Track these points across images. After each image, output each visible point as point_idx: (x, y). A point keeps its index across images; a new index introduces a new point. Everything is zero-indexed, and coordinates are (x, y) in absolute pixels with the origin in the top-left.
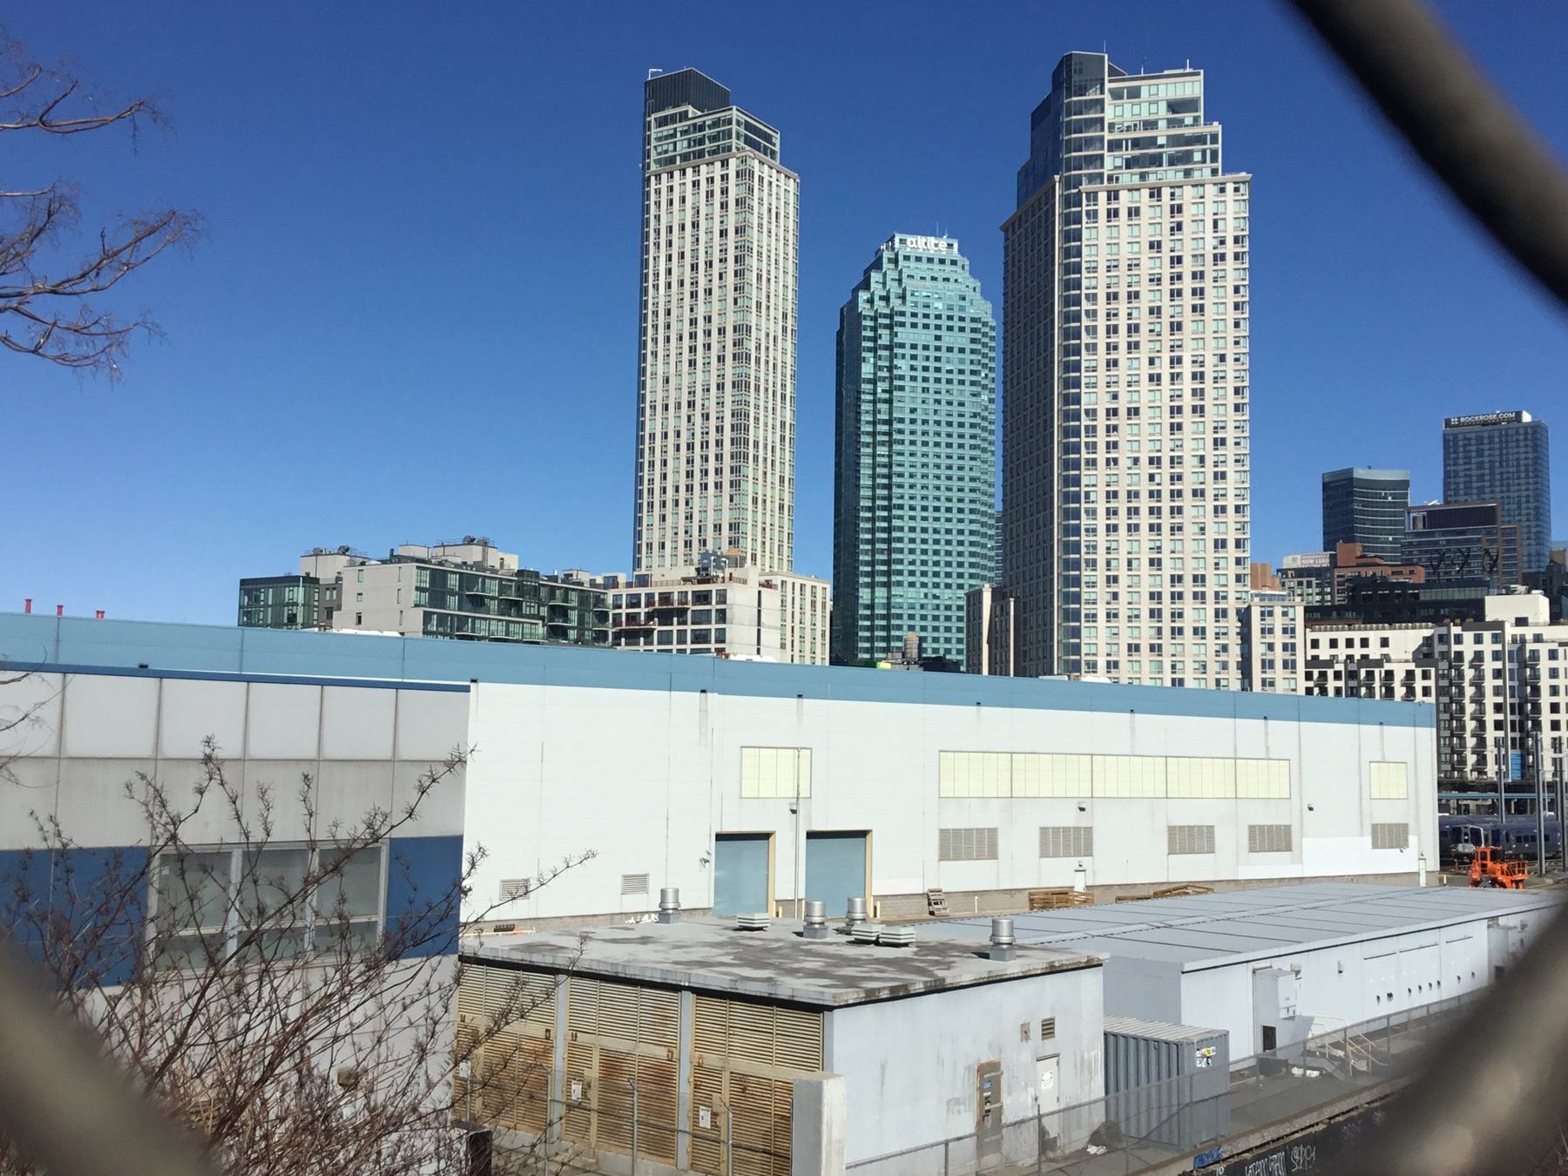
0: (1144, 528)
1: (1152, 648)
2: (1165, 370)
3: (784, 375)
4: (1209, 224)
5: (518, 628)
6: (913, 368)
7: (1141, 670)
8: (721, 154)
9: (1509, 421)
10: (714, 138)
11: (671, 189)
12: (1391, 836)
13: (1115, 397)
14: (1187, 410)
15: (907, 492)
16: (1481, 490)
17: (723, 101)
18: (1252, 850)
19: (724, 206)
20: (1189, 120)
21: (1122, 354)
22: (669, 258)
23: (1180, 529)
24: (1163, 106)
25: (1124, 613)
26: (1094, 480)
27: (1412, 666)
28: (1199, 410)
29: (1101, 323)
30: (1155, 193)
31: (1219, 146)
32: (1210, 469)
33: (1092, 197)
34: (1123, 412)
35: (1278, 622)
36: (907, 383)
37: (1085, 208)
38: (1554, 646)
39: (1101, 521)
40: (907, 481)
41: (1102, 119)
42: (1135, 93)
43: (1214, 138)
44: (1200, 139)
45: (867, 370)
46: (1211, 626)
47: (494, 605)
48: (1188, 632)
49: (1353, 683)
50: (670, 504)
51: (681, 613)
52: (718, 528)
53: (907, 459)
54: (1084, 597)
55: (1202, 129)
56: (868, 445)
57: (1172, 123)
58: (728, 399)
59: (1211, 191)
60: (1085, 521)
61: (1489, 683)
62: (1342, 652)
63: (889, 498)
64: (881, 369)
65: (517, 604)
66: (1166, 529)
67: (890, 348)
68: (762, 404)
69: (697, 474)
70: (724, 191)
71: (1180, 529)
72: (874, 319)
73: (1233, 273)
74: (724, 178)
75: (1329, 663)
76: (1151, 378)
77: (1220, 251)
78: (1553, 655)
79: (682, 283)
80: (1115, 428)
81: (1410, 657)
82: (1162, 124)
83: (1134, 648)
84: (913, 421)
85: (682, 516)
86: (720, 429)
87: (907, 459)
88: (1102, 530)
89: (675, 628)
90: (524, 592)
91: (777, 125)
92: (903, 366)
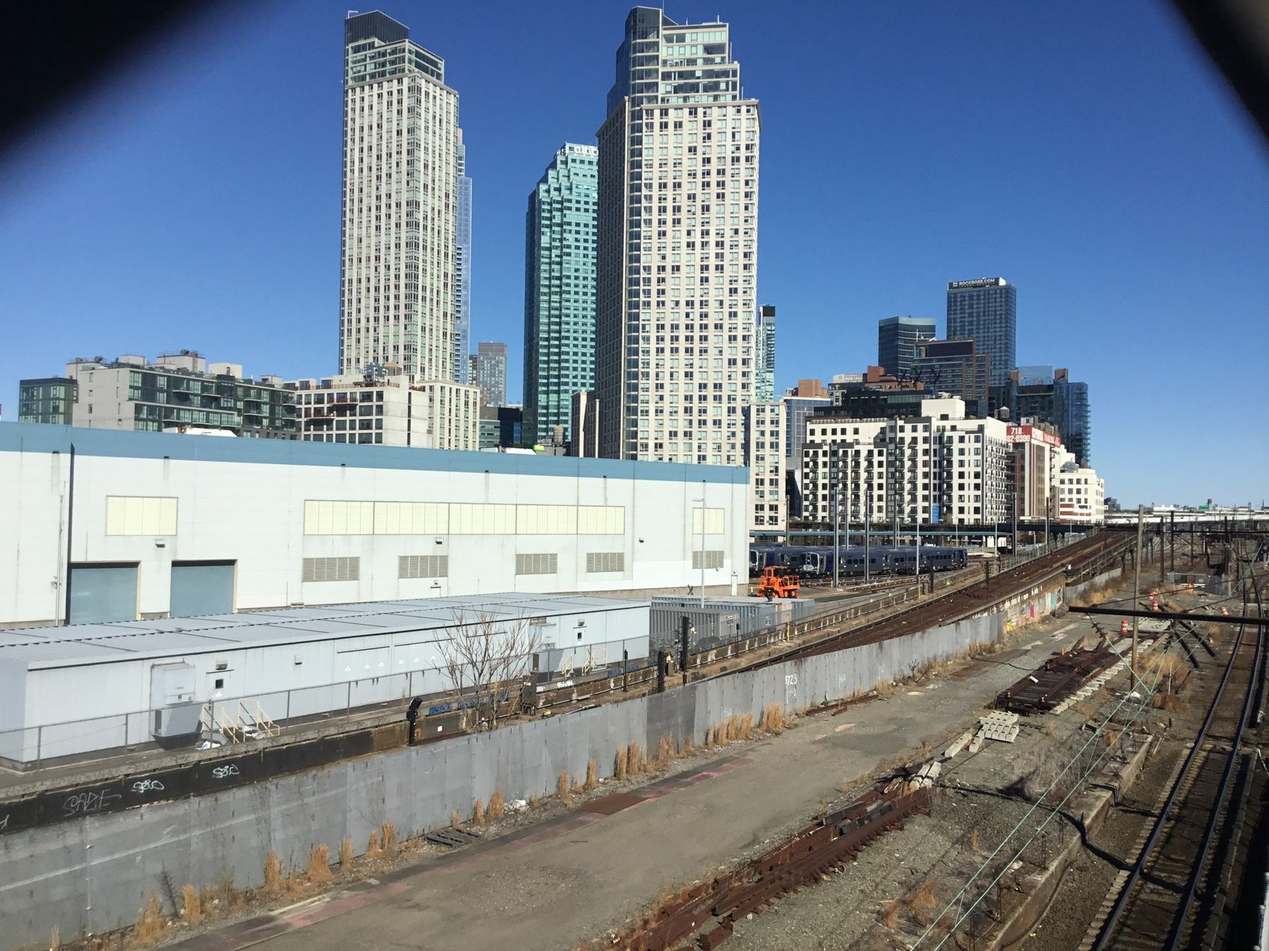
0: (682, 350)
1: (686, 434)
2: (698, 240)
3: (446, 239)
4: (729, 136)
5: (217, 417)
6: (577, 240)
7: (680, 452)
8: (398, 74)
9: (991, 284)
10: (393, 62)
11: (363, 99)
12: (715, 560)
13: (664, 258)
14: (712, 268)
15: (572, 327)
16: (971, 332)
17: (401, 34)
18: (590, 570)
19: (399, 112)
20: (718, 60)
21: (669, 227)
22: (362, 150)
23: (706, 351)
24: (701, 49)
25: (667, 410)
26: (649, 316)
27: (871, 447)
28: (720, 268)
29: (655, 205)
30: (693, 112)
31: (738, 79)
32: (726, 310)
33: (650, 113)
34: (669, 269)
35: (768, 416)
36: (573, 251)
37: (645, 121)
38: (963, 434)
39: (653, 346)
40: (572, 320)
41: (657, 57)
42: (681, 39)
43: (734, 75)
44: (725, 74)
45: (545, 241)
46: (725, 419)
47: (197, 400)
48: (710, 423)
49: (834, 459)
50: (363, 331)
51: (352, 408)
52: (396, 348)
53: (572, 304)
54: (640, 398)
55: (727, 66)
56: (545, 294)
57: (707, 61)
58: (403, 255)
59: (731, 111)
60: (642, 345)
61: (921, 458)
62: (829, 438)
63: (559, 332)
64: (554, 240)
65: (217, 399)
66: (696, 351)
67: (561, 225)
68: (429, 260)
69: (382, 309)
70: (400, 102)
71: (706, 351)
72: (550, 204)
73: (749, 172)
74: (400, 92)
75: (820, 446)
76: (688, 245)
77: (736, 155)
78: (962, 439)
79: (370, 169)
80: (664, 280)
81: (872, 441)
82: (700, 62)
83: (673, 434)
84: (577, 278)
85: (372, 339)
86: (397, 277)
87: (572, 304)
88: (653, 352)
89: (348, 418)
90: (221, 391)
91: (441, 55)
92: (570, 238)
